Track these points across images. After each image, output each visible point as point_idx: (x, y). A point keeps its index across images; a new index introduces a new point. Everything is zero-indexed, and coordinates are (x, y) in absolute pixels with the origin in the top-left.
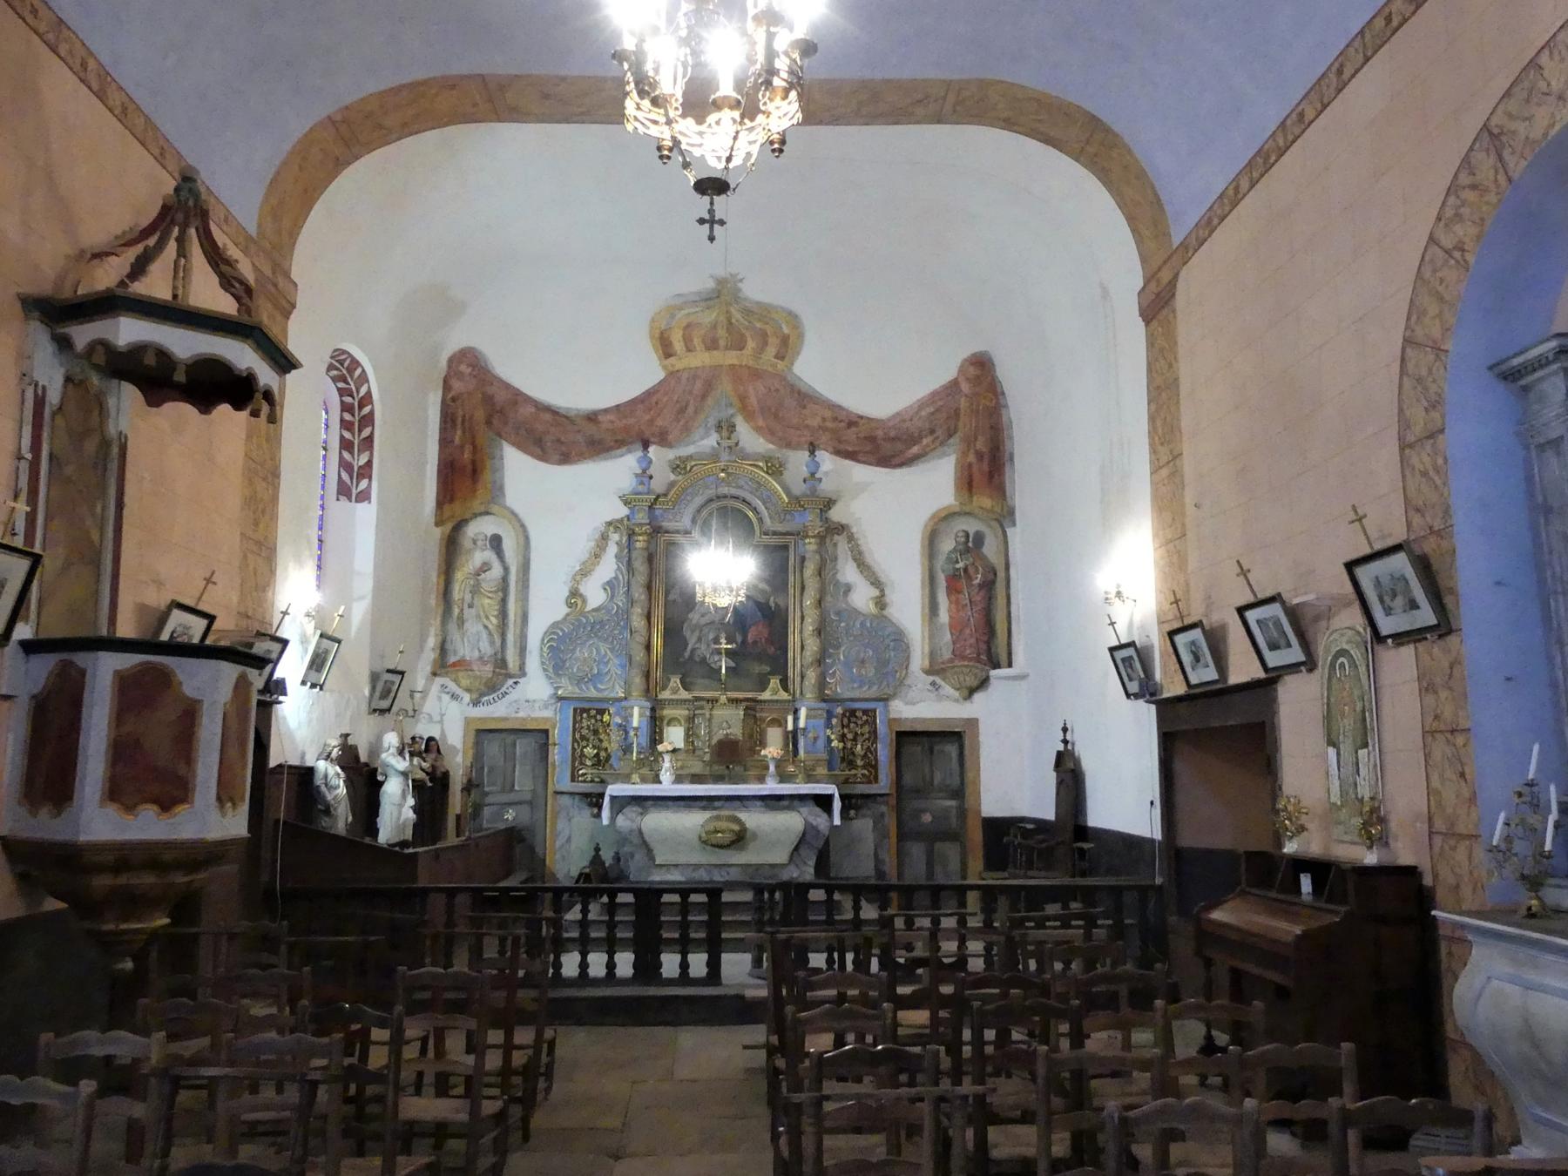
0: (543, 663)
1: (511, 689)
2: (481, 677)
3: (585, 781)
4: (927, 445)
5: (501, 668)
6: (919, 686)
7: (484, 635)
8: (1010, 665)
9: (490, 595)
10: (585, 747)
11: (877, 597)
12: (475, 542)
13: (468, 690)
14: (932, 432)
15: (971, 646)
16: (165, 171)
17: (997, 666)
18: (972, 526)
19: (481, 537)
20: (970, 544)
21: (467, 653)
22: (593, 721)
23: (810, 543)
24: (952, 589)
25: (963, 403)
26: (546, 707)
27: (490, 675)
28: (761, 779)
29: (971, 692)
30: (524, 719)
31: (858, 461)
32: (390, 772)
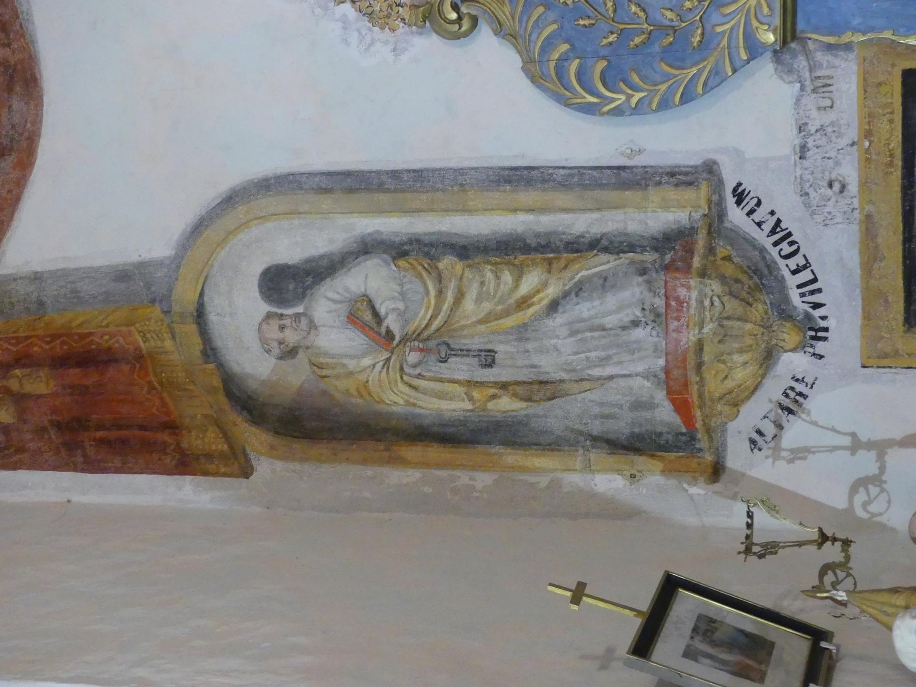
0: (665, 104)
2: (722, 320)
7: (584, 309)
9: (450, 296)
12: (290, 353)
13: (769, 358)
16: (898, 435)
26: (822, 87)
27: (715, 286)
30: (867, 161)
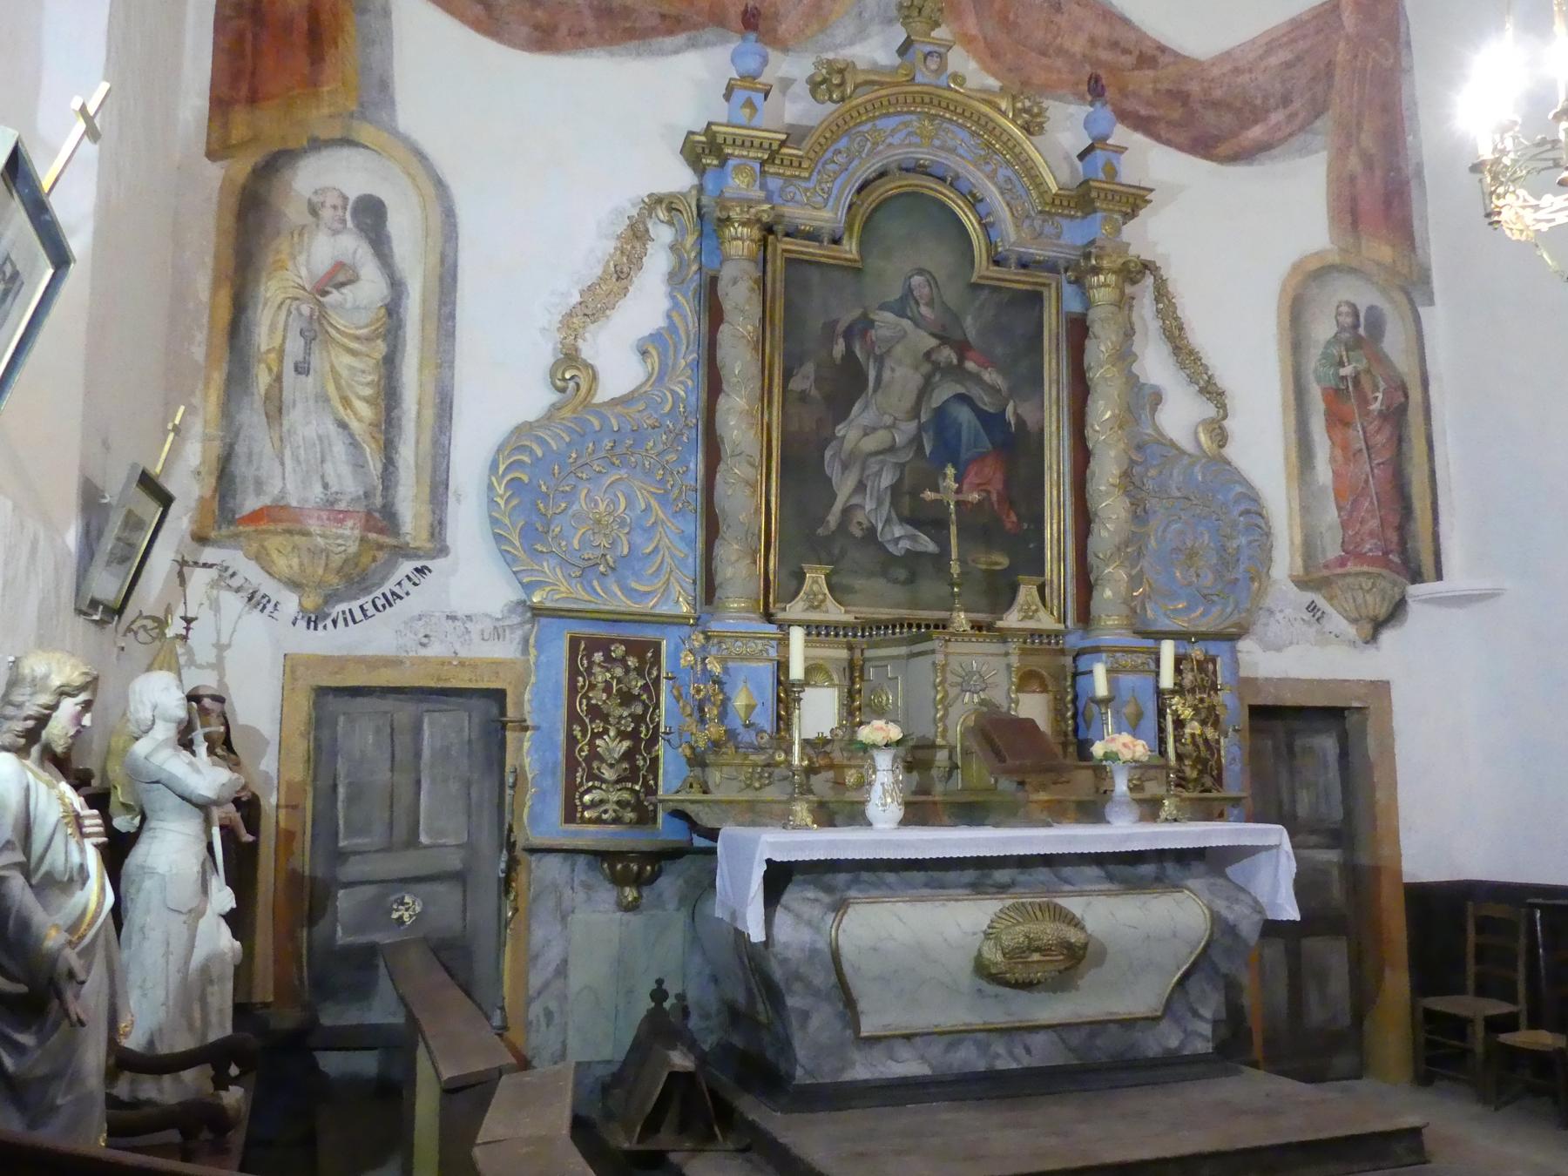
0: (494, 521)
1: (407, 585)
3: (598, 821)
4: (1278, 127)
5: (381, 531)
6: (1288, 611)
7: (339, 449)
8: (1439, 577)
9: (355, 345)
10: (600, 735)
11: (1213, 421)
12: (314, 211)
13: (294, 585)
14: (1286, 101)
15: (1371, 534)
17: (1416, 577)
18: (1365, 297)
19: (331, 199)
20: (1361, 331)
21: (290, 487)
22: (619, 672)
23: (1105, 285)
24: (1337, 420)
25: (1342, 53)
26: (498, 633)
28: (1092, 810)
29: (1376, 626)
31: (1158, 138)
32: (162, 800)
